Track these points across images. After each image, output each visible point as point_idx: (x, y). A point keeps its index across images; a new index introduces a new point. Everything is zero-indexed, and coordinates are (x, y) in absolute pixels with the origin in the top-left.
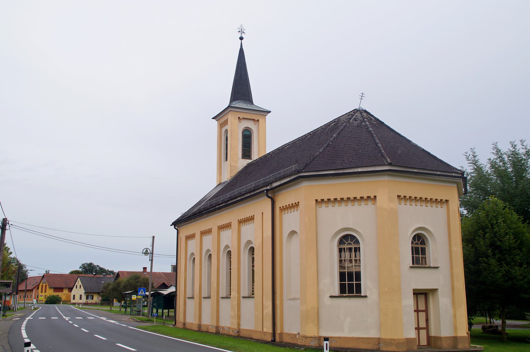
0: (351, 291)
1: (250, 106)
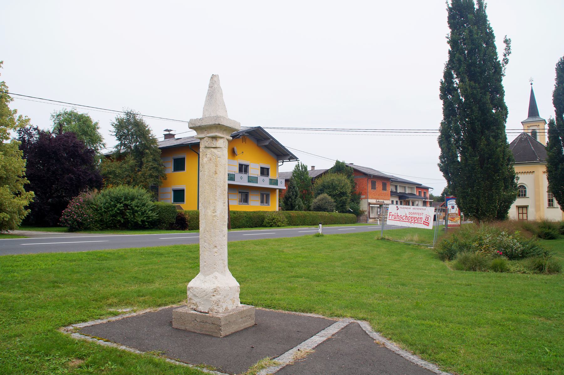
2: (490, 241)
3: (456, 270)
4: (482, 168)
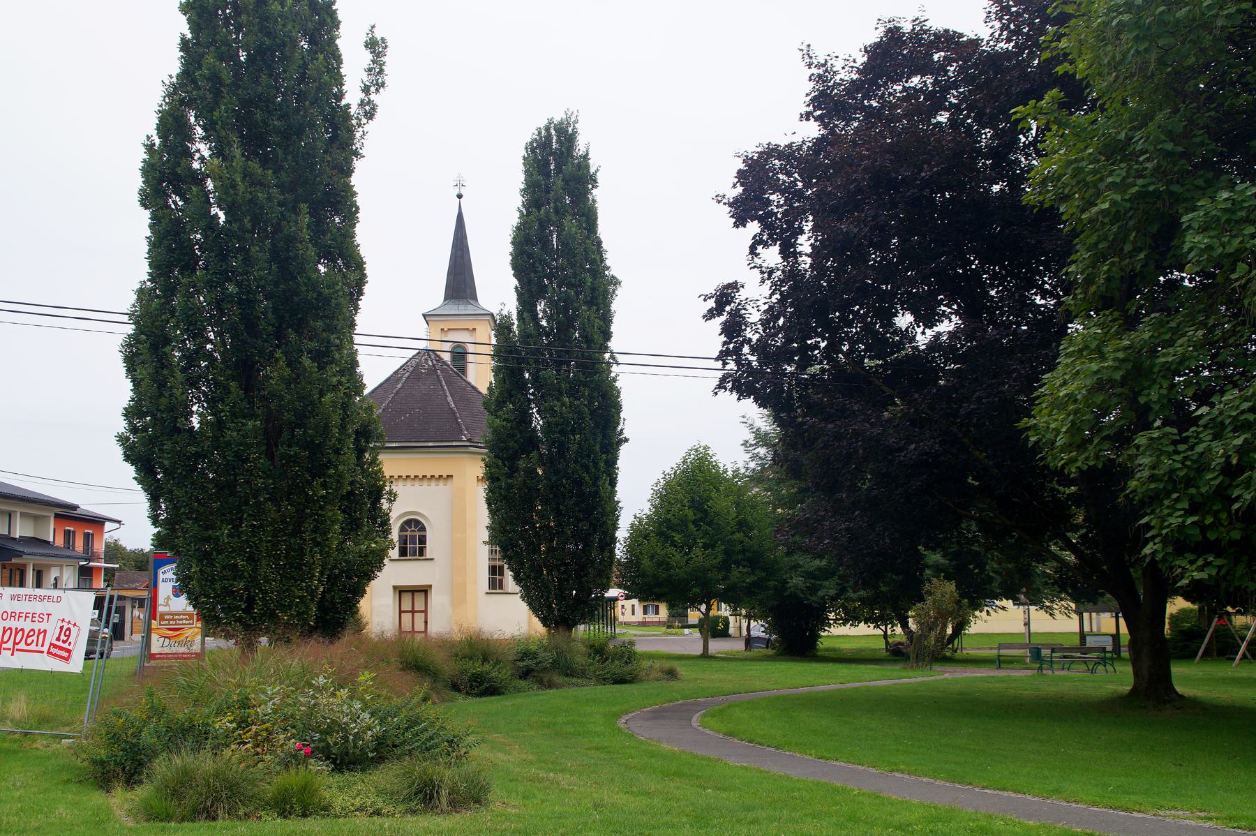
1: (456, 307)
2: (275, 711)
3: (148, 820)
4: (271, 456)
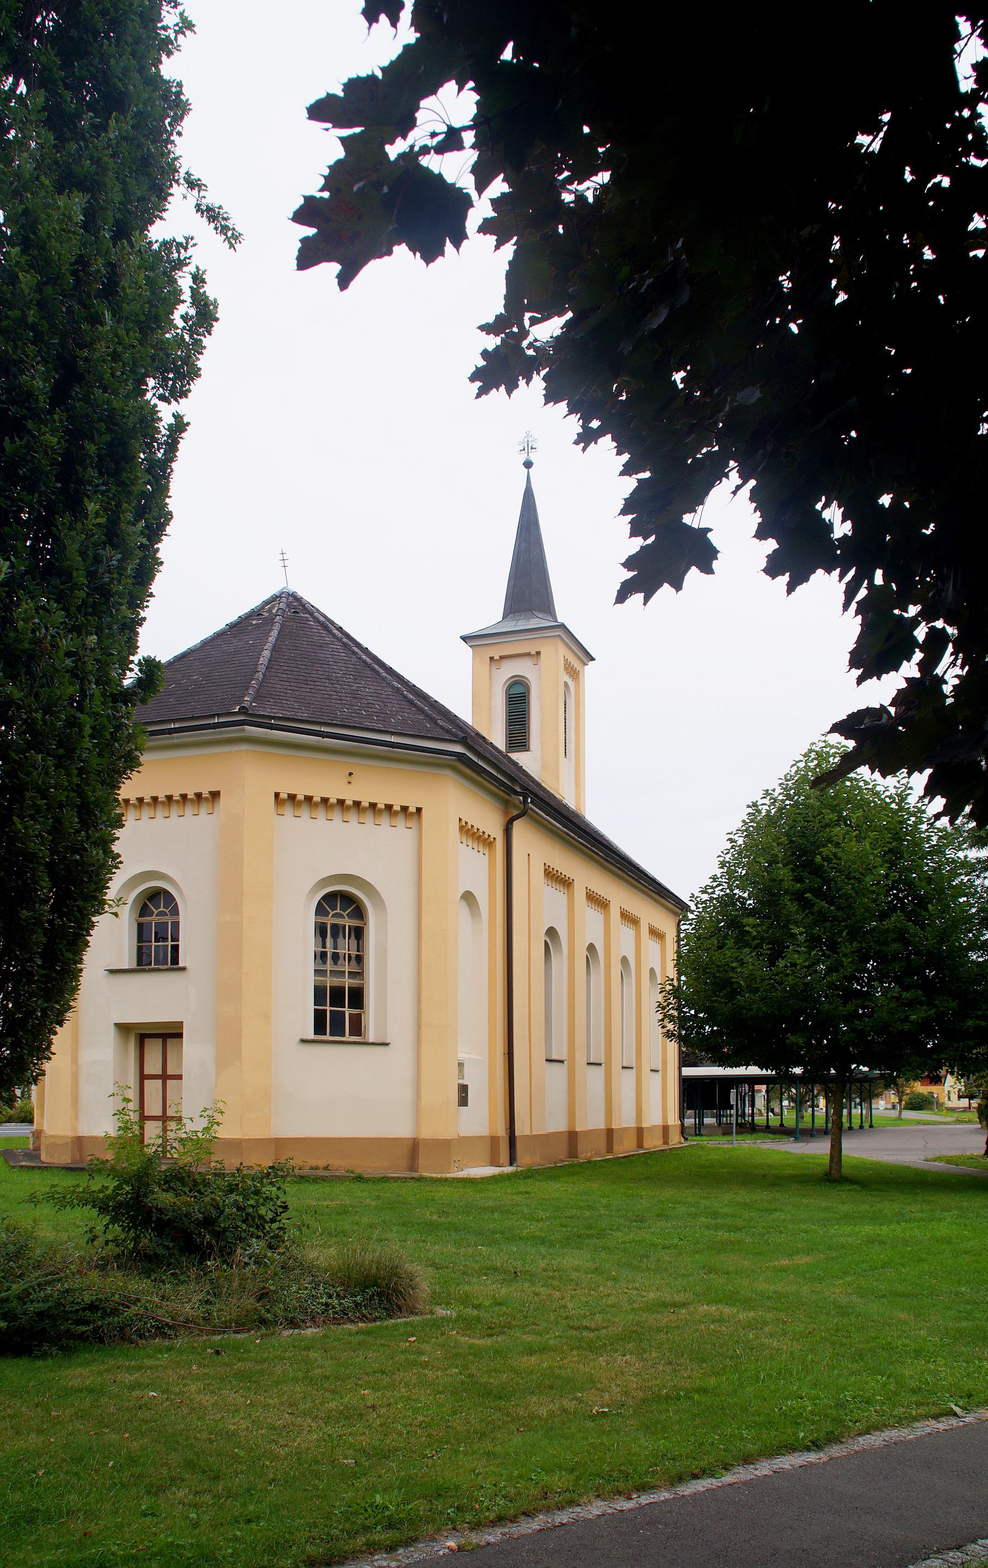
0: (338, 1029)
